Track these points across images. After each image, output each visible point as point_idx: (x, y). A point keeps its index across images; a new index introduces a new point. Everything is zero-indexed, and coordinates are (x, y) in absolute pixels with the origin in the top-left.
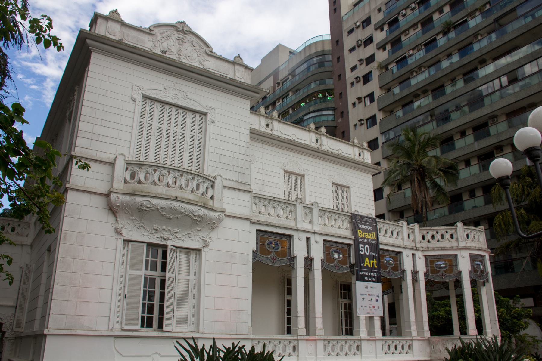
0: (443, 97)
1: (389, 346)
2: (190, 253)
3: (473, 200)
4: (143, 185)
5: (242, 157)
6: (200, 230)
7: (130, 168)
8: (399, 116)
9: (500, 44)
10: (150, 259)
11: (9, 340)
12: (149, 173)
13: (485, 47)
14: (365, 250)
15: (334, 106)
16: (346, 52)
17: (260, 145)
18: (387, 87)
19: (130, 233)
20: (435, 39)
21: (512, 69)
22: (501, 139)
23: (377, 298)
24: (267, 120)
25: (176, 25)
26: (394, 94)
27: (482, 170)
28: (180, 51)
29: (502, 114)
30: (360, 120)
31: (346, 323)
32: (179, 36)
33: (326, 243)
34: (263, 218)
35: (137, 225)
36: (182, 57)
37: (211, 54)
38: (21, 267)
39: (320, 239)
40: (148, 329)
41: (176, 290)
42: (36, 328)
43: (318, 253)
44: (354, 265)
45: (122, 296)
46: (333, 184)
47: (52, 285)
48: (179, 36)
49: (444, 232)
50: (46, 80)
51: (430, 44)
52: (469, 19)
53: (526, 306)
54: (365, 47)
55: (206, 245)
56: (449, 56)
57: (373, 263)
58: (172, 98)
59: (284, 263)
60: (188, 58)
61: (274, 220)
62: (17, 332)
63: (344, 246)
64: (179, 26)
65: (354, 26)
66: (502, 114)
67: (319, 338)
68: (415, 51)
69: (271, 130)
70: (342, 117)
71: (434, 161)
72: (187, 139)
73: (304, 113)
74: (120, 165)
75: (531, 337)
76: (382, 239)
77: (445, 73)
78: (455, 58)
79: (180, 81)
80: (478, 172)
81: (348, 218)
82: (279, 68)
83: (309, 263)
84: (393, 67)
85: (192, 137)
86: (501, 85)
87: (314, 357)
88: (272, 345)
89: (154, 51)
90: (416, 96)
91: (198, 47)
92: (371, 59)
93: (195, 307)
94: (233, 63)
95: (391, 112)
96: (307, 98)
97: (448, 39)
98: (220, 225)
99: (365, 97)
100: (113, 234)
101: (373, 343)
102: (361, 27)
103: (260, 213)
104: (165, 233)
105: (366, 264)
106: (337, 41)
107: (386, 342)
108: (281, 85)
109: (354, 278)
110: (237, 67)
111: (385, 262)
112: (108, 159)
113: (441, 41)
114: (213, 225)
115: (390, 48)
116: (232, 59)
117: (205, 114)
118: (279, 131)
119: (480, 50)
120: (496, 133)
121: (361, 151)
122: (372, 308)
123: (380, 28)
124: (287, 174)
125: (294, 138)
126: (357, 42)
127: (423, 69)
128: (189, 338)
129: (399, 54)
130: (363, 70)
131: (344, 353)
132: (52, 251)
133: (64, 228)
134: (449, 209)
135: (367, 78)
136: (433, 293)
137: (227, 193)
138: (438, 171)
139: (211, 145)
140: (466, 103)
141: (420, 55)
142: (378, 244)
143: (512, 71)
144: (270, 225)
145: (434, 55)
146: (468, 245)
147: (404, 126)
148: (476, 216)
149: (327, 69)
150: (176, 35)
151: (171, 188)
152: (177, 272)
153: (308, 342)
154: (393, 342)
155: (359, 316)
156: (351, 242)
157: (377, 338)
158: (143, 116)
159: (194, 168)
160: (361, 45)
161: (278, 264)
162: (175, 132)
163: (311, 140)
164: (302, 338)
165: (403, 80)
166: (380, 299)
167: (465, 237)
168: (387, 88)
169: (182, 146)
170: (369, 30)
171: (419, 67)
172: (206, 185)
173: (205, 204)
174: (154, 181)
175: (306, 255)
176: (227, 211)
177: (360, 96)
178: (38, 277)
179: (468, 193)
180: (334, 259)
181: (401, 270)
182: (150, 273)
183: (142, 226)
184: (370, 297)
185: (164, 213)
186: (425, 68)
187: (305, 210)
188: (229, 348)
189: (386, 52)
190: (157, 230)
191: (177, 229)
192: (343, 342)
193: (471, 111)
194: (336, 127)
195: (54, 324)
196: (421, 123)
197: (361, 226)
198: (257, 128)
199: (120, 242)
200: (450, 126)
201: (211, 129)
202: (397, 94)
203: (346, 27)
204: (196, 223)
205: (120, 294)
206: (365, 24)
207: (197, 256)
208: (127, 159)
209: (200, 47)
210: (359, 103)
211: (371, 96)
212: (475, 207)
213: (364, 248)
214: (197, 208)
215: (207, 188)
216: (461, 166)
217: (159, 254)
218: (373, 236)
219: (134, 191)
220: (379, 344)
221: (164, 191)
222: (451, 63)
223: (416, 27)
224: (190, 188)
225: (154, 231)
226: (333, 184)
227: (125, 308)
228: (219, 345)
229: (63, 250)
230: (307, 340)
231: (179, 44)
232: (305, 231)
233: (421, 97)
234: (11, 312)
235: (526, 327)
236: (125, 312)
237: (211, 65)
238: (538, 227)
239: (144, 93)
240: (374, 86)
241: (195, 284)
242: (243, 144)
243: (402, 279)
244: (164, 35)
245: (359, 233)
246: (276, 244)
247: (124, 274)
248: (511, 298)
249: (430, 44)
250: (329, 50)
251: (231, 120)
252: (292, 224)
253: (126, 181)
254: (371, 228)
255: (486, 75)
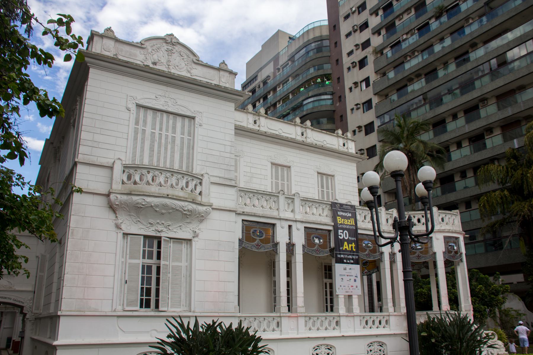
0: (436, 80)
1: (373, 321)
2: (182, 243)
3: (464, 181)
4: (138, 185)
5: (228, 155)
6: (190, 223)
7: (126, 170)
8: (394, 100)
9: (490, 27)
10: (147, 249)
11: (30, 321)
12: (143, 175)
13: (476, 31)
14: (343, 235)
15: (332, 90)
16: (343, 37)
17: (248, 140)
18: (382, 71)
19: (129, 228)
20: (428, 24)
21: (501, 53)
22: (491, 121)
23: (356, 278)
24: (255, 117)
25: (165, 37)
26: (388, 79)
27: (473, 152)
28: (169, 61)
29: (492, 97)
30: (357, 105)
31: (328, 302)
32: (168, 47)
33: (307, 230)
34: (247, 210)
35: (135, 220)
36: (171, 67)
37: (198, 63)
38: (37, 257)
39: (301, 227)
40: (146, 309)
41: (170, 275)
42: (52, 310)
43: (299, 239)
44: (334, 249)
45: (123, 282)
46: (318, 173)
47: (63, 274)
48: (168, 47)
49: (420, 217)
50: (59, 71)
51: (424, 28)
52: (461, 3)
53: (506, 282)
54: (361, 32)
55: (196, 235)
56: (442, 40)
57: (352, 247)
58: (163, 106)
59: (268, 248)
60: (177, 67)
61: (258, 211)
62: (37, 313)
63: (324, 231)
64: (167, 39)
65: (350, 11)
66: (492, 97)
67: (301, 315)
68: (409, 36)
69: (259, 126)
70: (340, 101)
71: (422, 147)
72: (178, 142)
73: (304, 98)
74: (118, 168)
75: (515, 311)
76: (360, 224)
77: (437, 57)
78: (448, 42)
79: (170, 89)
80: (469, 153)
81: (328, 206)
82: (279, 53)
83: (291, 248)
84: (388, 52)
85: (182, 139)
86: (491, 69)
87: (296, 332)
88: (247, 321)
89: (146, 64)
90: (410, 79)
91: (186, 57)
92: (366, 44)
93: (188, 289)
94: (219, 69)
95: (387, 96)
96: (307, 83)
97: (441, 23)
98: (209, 217)
99: (361, 82)
100: (114, 229)
101: (351, 319)
102: (357, 12)
103: (245, 204)
104: (159, 226)
105: (344, 247)
106: (335, 26)
107: (364, 318)
108: (281, 70)
109: (334, 260)
110: (222, 73)
111: (364, 245)
112: (108, 163)
113: (434, 25)
114: (201, 218)
115: (385, 32)
116: (217, 65)
117: (193, 118)
118: (266, 126)
119: (472, 33)
120: (486, 115)
121: (345, 141)
122: (350, 287)
123: (375, 12)
124: (274, 166)
125: (281, 132)
126: (353, 27)
127: (416, 54)
128: (177, 317)
129: (394, 39)
130: (359, 55)
131: (324, 328)
132: (62, 244)
133: (71, 225)
134: (442, 190)
135: (362, 63)
136: (420, 271)
137: (214, 188)
138: (425, 156)
139: (199, 145)
140: (457, 86)
141: (413, 39)
142: (357, 229)
143: (501, 55)
144: (255, 215)
145: (426, 40)
146: (443, 228)
147: (398, 110)
148: (466, 196)
149: (325, 54)
150: (165, 47)
151: (163, 187)
152: (171, 260)
153: (290, 318)
154: (370, 318)
155: (338, 295)
156: (331, 228)
157: (355, 314)
158: (137, 123)
159: (184, 169)
160: (356, 30)
161: (262, 250)
162: (167, 136)
163: (296, 134)
164: (285, 315)
165: (398, 64)
166: (359, 279)
167: (440, 220)
168: (382, 72)
169: (173, 149)
170: (365, 15)
171: (413, 51)
172: (194, 182)
173: (193, 200)
174: (148, 181)
175: (288, 241)
176: (214, 204)
177: (356, 80)
178: (52, 265)
179: (459, 175)
180: (315, 244)
181: (379, 252)
182: (148, 261)
183: (139, 221)
184: (349, 278)
185: (157, 209)
186: (418, 52)
187: (287, 200)
188: (210, 324)
189: (381, 36)
190: (152, 224)
191: (170, 223)
192: (323, 318)
193: (462, 94)
194: (334, 111)
195: (67, 305)
196: (415, 106)
197: (340, 213)
198: (245, 125)
199: (120, 235)
200: (442, 109)
201: (199, 132)
202: (392, 78)
203: (343, 12)
204: (186, 216)
205: (121, 280)
206: (360, 9)
207: (189, 246)
208: (124, 163)
209: (188, 56)
210: (355, 88)
211: (367, 80)
212: (466, 188)
213: (343, 233)
214: (187, 203)
215: (196, 185)
216: (453, 148)
217: (154, 244)
218: (351, 222)
219: (131, 191)
220: (357, 320)
221: (157, 189)
222: (443, 47)
223: (409, 11)
224: (180, 186)
225: (149, 225)
226: (318, 173)
227: (126, 292)
228: (201, 322)
229: (71, 244)
230: (289, 317)
231: (168, 55)
232: (287, 220)
233: (415, 81)
234: (30, 296)
235: (504, 302)
236: (126, 295)
237: (199, 74)
238: (523, 208)
239: (137, 102)
240: (369, 71)
241: (187, 269)
242: (229, 143)
243: (381, 260)
244: (154, 48)
245: (338, 220)
246: (260, 232)
247: (124, 263)
248: (490, 275)
249: (424, 28)
250: (327, 36)
251: (217, 121)
252: (275, 214)
253: (123, 183)
254: (350, 215)
255: (476, 59)
